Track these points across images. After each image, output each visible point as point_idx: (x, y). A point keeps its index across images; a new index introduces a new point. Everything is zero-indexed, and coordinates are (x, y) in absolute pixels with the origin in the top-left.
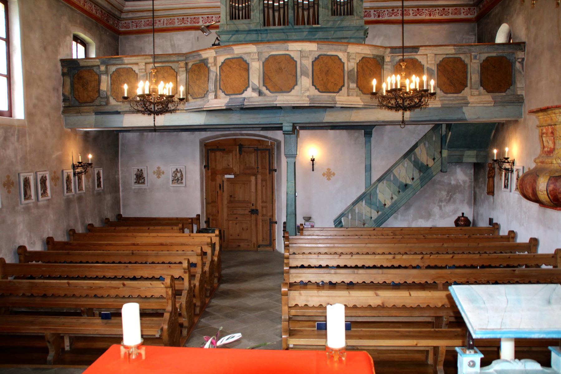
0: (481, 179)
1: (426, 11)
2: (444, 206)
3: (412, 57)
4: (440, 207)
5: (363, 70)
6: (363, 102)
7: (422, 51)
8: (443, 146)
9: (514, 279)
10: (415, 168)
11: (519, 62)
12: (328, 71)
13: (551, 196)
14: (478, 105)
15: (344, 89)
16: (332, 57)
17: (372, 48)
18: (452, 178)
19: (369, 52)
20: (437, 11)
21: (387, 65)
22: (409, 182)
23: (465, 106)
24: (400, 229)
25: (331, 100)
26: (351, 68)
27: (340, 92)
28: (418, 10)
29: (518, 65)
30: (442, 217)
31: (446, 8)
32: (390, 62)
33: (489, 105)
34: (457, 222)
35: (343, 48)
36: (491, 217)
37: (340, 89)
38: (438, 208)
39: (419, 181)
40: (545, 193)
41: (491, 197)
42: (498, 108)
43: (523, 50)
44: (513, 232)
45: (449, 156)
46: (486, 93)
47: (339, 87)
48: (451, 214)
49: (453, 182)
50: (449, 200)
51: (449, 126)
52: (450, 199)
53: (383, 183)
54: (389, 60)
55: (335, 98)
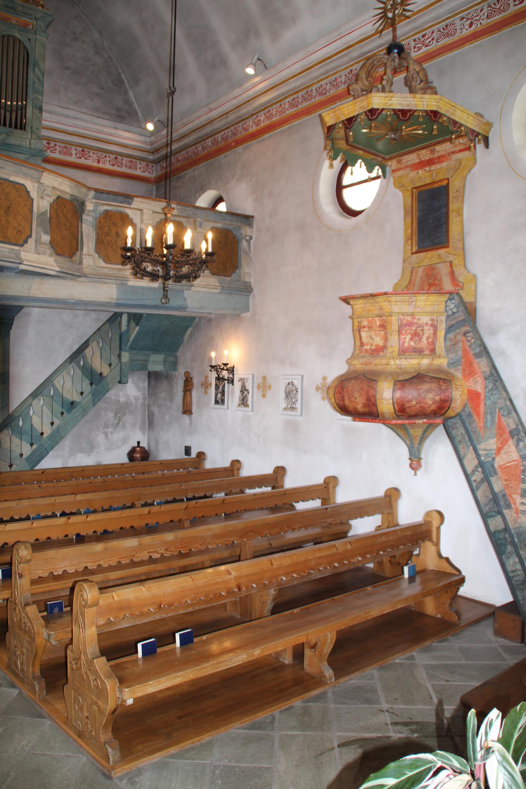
0: (163, 394)
1: (94, 156)
2: (111, 432)
3: (122, 209)
4: (106, 434)
5: (58, 216)
6: (59, 267)
7: (137, 203)
8: (123, 346)
9: (327, 520)
10: (84, 377)
11: (246, 240)
12: (9, 207)
13: (397, 405)
14: (203, 290)
15: (31, 242)
16: (18, 186)
17: (73, 184)
18: (121, 393)
19: (68, 190)
20: (108, 159)
21: (88, 215)
22: (76, 398)
23: (187, 290)
24: (41, 471)
25: (13, 256)
26: (44, 210)
27: (25, 245)
28: (83, 151)
29: (244, 244)
30: (109, 449)
31: (119, 157)
32: (93, 211)
33: (215, 291)
34: (131, 455)
35: (35, 174)
36: (188, 445)
37: (26, 242)
38: (103, 436)
39: (90, 396)
40: (391, 402)
41: (186, 418)
42: (223, 297)
43: (250, 225)
44: (238, 461)
45: (131, 360)
46: (210, 275)
47: (24, 237)
48: (120, 443)
49: (122, 399)
50: (118, 423)
51: (135, 318)
52: (118, 424)
53: (40, 400)
54: (91, 209)
55: (19, 254)
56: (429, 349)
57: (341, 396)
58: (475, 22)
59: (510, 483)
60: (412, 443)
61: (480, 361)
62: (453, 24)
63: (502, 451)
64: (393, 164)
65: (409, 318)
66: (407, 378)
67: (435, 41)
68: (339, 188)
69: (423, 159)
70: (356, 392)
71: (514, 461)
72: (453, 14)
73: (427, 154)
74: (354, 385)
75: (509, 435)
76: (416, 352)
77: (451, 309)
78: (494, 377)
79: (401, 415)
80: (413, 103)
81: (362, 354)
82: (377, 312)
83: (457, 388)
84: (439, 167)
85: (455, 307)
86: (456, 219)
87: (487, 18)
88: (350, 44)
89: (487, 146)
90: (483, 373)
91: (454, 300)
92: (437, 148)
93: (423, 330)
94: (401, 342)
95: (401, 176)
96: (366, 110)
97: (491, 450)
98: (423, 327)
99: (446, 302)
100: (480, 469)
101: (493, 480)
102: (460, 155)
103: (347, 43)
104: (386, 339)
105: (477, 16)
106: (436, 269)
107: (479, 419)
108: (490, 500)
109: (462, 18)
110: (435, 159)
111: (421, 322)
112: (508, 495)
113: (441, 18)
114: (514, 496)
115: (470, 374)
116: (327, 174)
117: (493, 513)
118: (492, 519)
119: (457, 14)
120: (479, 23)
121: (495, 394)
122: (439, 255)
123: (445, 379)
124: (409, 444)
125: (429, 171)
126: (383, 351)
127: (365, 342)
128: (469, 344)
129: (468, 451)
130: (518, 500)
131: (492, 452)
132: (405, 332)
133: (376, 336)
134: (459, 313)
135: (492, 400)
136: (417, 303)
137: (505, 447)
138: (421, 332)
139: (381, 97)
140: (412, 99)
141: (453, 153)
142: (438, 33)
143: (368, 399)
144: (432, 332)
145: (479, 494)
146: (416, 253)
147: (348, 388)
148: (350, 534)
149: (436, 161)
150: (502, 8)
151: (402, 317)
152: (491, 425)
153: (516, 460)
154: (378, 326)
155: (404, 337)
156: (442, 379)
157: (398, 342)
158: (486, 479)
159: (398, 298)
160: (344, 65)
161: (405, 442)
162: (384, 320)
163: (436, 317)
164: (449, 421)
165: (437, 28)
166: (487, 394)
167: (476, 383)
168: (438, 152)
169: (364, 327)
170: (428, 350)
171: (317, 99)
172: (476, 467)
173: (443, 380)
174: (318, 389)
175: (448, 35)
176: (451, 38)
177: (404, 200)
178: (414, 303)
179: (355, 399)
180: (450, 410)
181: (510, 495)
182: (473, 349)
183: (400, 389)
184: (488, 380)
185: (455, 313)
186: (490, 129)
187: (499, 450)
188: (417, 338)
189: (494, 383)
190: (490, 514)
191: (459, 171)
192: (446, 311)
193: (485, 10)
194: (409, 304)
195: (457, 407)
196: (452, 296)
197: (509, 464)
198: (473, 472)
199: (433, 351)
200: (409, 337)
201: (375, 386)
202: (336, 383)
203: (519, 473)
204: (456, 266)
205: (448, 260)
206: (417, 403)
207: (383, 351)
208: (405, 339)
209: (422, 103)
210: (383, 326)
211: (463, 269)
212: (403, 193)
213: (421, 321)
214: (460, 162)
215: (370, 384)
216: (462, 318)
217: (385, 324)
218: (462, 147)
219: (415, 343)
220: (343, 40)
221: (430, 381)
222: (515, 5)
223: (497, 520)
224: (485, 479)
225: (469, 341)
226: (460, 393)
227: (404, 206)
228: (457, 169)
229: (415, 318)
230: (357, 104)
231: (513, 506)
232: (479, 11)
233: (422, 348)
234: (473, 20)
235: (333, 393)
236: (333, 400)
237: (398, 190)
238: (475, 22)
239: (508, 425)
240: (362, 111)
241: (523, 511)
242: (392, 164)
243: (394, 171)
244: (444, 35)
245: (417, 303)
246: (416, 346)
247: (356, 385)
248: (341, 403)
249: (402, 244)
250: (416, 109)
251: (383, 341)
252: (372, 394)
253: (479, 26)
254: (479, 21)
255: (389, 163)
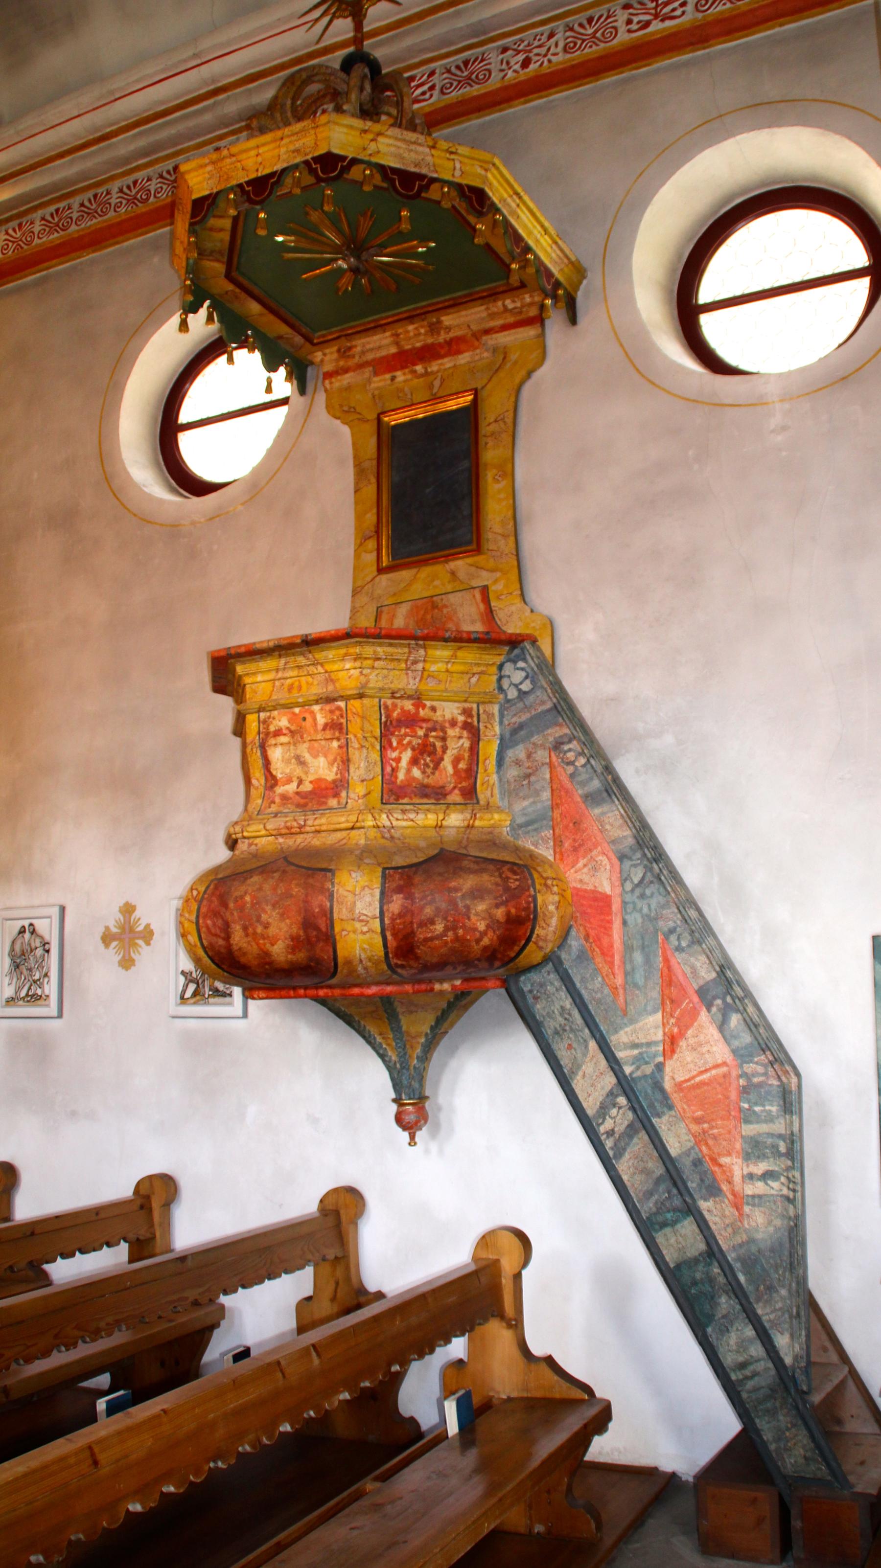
13: (394, 935)
56: (461, 789)
57: (220, 922)
58: (535, 59)
59: (712, 1128)
60: (404, 1057)
61: (603, 813)
62: (482, 60)
63: (683, 1043)
64: (327, 358)
65: (408, 705)
66: (416, 860)
67: (436, 93)
68: (168, 428)
69: (408, 347)
70: (268, 908)
71: (717, 1066)
72: (483, 38)
73: (420, 334)
74: (260, 889)
75: (696, 999)
76: (426, 796)
77: (516, 686)
78: (648, 848)
79: (402, 966)
80: (429, 159)
81: (274, 808)
82: (317, 690)
83: (546, 885)
84: (448, 365)
85: (526, 677)
86: (497, 486)
87: (565, 50)
88: (219, 84)
89: (573, 319)
90: (613, 842)
91: (524, 660)
92: (447, 320)
93: (444, 739)
94: (388, 769)
95: (349, 388)
96: (309, 157)
97: (649, 1044)
98: (443, 730)
99: (501, 667)
100: (622, 1100)
101: (662, 1124)
102: (504, 339)
103: (213, 81)
104: (346, 762)
105: (539, 46)
106: (446, 606)
107: (611, 964)
108: (658, 1181)
109: (505, 50)
110: (440, 345)
111: (438, 716)
112: (708, 1164)
113: (452, 43)
114: (724, 1160)
115: (575, 850)
116: (166, 345)
117: (669, 1216)
118: (668, 1230)
119: (492, 40)
120: (546, 60)
121: (652, 895)
122: (453, 573)
123: (514, 864)
124: (394, 1058)
125: (422, 376)
126: (336, 795)
127: (279, 776)
128: (570, 769)
129: (585, 1055)
130: (737, 1167)
131: (653, 1049)
132: (400, 742)
133: (315, 756)
134: (539, 693)
135: (645, 910)
136: (427, 666)
137: (690, 1032)
138: (438, 744)
139: (351, 127)
140: (427, 150)
141: (487, 332)
142: (445, 76)
143: (308, 924)
144: (467, 744)
145: (624, 1167)
146: (390, 569)
147: (242, 897)
148: (218, 1349)
149: (442, 352)
150: (599, 35)
151: (389, 702)
152: (647, 978)
153: (724, 1064)
154: (320, 727)
155: (394, 755)
156: (506, 863)
157: (378, 769)
158: (643, 1123)
159: (379, 649)
160: (199, 136)
161: (382, 1056)
162: (339, 708)
163: (475, 706)
164: (522, 978)
165: (441, 66)
166: (628, 898)
167: (595, 869)
168: (448, 329)
169: (278, 733)
170: (457, 791)
171: (123, 210)
172: (611, 1094)
173: (508, 866)
174: (107, 938)
175: (469, 81)
176: (476, 87)
177: (354, 444)
178: (420, 666)
179: (266, 926)
180: (531, 946)
181: (714, 1161)
182: (583, 784)
183: (399, 890)
184: (630, 859)
185: (525, 693)
186: (580, 282)
187: (672, 1043)
188: (428, 759)
189: (645, 867)
190: (660, 1219)
191: (502, 374)
192: (501, 689)
193: (559, 36)
194: (408, 669)
195: (550, 937)
196: (517, 651)
197: (705, 1076)
198: (603, 1111)
199: (470, 793)
200: (407, 756)
201: (328, 885)
202: (202, 889)
203: (733, 1095)
204: (498, 598)
205: (477, 583)
206: (447, 929)
207: (336, 795)
208: (398, 760)
209: (451, 164)
210: (336, 727)
211: (519, 604)
212: (350, 427)
213: (439, 713)
214: (504, 353)
215: (311, 881)
216: (549, 705)
217: (343, 721)
218: (511, 320)
219: (424, 772)
220: (205, 71)
221: (476, 867)
222: (629, 31)
223: (683, 1231)
224: (638, 1125)
225: (572, 763)
226: (556, 898)
227: (356, 457)
228: (497, 371)
229: (424, 707)
230: (285, 141)
231: (725, 1187)
232: (544, 38)
233: (443, 787)
234: (531, 55)
235: (193, 918)
236: (193, 938)
237: (338, 422)
238: (535, 59)
239: (694, 971)
240: (298, 160)
241: (753, 1196)
242: (326, 358)
243: (328, 375)
244: (460, 82)
245: (427, 666)
246: (426, 781)
247: (266, 887)
248: (221, 942)
249: (349, 551)
250: (435, 175)
251: (335, 769)
252: (320, 906)
253: (546, 63)
254: (545, 56)
255: (318, 356)
